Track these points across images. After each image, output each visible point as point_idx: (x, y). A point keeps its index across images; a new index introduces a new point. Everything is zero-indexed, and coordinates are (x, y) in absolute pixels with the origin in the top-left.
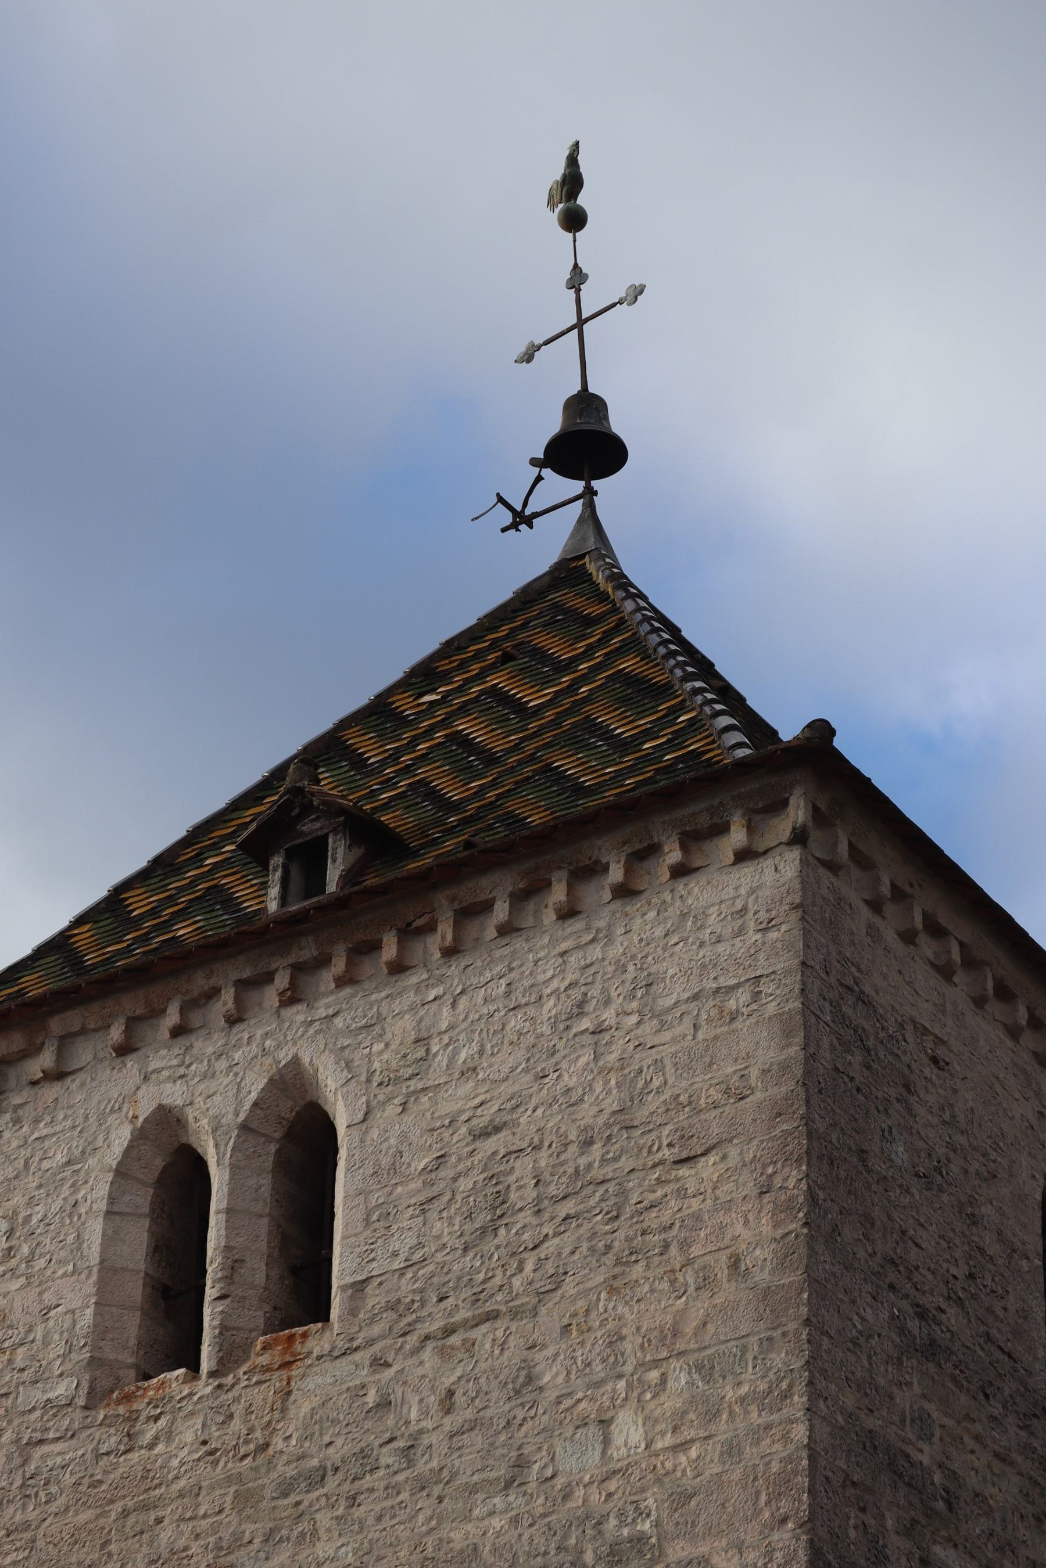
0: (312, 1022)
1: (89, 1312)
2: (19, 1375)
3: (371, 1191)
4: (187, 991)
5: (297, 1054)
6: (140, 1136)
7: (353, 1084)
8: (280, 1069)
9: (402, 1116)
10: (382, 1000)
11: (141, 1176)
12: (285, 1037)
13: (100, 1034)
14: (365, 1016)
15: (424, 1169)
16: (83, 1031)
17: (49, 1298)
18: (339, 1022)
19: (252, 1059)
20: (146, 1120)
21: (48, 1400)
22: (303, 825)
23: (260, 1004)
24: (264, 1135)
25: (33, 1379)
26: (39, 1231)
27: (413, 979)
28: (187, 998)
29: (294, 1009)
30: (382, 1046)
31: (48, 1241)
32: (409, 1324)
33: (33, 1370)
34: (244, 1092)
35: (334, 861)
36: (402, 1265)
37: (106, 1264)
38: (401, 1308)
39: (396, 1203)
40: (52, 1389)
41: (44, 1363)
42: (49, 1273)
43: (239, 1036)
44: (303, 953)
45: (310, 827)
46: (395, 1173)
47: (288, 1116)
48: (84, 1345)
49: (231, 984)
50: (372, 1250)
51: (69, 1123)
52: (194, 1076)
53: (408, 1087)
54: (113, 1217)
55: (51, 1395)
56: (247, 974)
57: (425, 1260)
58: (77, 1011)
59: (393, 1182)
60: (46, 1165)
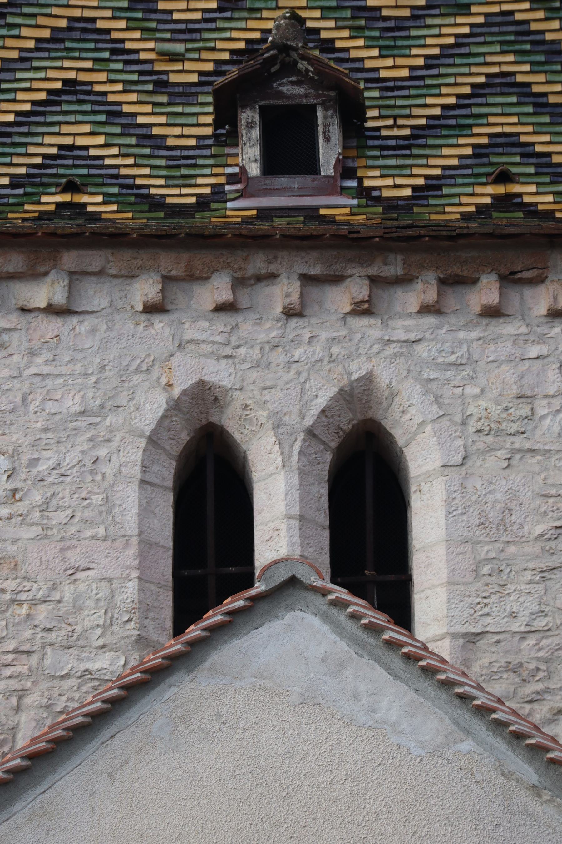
0: (389, 342)
1: (132, 586)
2: (44, 634)
3: (479, 542)
4: (240, 269)
5: (372, 371)
6: (175, 406)
7: (445, 423)
8: (352, 382)
9: (507, 471)
10: (473, 340)
11: (168, 447)
12: (357, 349)
13: (120, 280)
14: (453, 353)
15: (542, 535)
16: (100, 273)
17: (75, 558)
18: (422, 350)
19: (317, 361)
20: (184, 393)
21: (86, 670)
22: (282, 84)
23: (320, 303)
24: (324, 443)
25: (65, 643)
26: (51, 479)
27: (509, 328)
28: (238, 275)
29: (365, 321)
30: (477, 391)
31: (67, 493)
32: (538, 693)
33: (63, 633)
34: (308, 395)
35: (327, 139)
36: (523, 629)
37: (143, 536)
38: (525, 674)
39: (510, 562)
40: (89, 659)
41: (78, 629)
42: (73, 530)
43: (299, 332)
44: (387, 268)
45: (292, 90)
46: (506, 530)
47: (345, 427)
48: (129, 620)
49: (296, 276)
50: (486, 605)
51: (78, 367)
52: (244, 361)
53: (513, 443)
54: (145, 486)
55: (90, 666)
56: (316, 270)
57: (549, 630)
58: (100, 253)
59: (504, 538)
60: (51, 407)
